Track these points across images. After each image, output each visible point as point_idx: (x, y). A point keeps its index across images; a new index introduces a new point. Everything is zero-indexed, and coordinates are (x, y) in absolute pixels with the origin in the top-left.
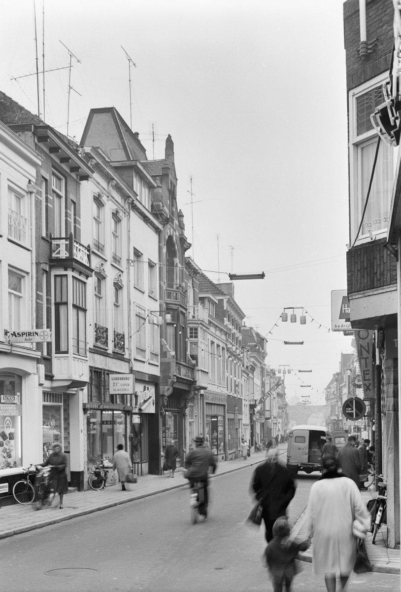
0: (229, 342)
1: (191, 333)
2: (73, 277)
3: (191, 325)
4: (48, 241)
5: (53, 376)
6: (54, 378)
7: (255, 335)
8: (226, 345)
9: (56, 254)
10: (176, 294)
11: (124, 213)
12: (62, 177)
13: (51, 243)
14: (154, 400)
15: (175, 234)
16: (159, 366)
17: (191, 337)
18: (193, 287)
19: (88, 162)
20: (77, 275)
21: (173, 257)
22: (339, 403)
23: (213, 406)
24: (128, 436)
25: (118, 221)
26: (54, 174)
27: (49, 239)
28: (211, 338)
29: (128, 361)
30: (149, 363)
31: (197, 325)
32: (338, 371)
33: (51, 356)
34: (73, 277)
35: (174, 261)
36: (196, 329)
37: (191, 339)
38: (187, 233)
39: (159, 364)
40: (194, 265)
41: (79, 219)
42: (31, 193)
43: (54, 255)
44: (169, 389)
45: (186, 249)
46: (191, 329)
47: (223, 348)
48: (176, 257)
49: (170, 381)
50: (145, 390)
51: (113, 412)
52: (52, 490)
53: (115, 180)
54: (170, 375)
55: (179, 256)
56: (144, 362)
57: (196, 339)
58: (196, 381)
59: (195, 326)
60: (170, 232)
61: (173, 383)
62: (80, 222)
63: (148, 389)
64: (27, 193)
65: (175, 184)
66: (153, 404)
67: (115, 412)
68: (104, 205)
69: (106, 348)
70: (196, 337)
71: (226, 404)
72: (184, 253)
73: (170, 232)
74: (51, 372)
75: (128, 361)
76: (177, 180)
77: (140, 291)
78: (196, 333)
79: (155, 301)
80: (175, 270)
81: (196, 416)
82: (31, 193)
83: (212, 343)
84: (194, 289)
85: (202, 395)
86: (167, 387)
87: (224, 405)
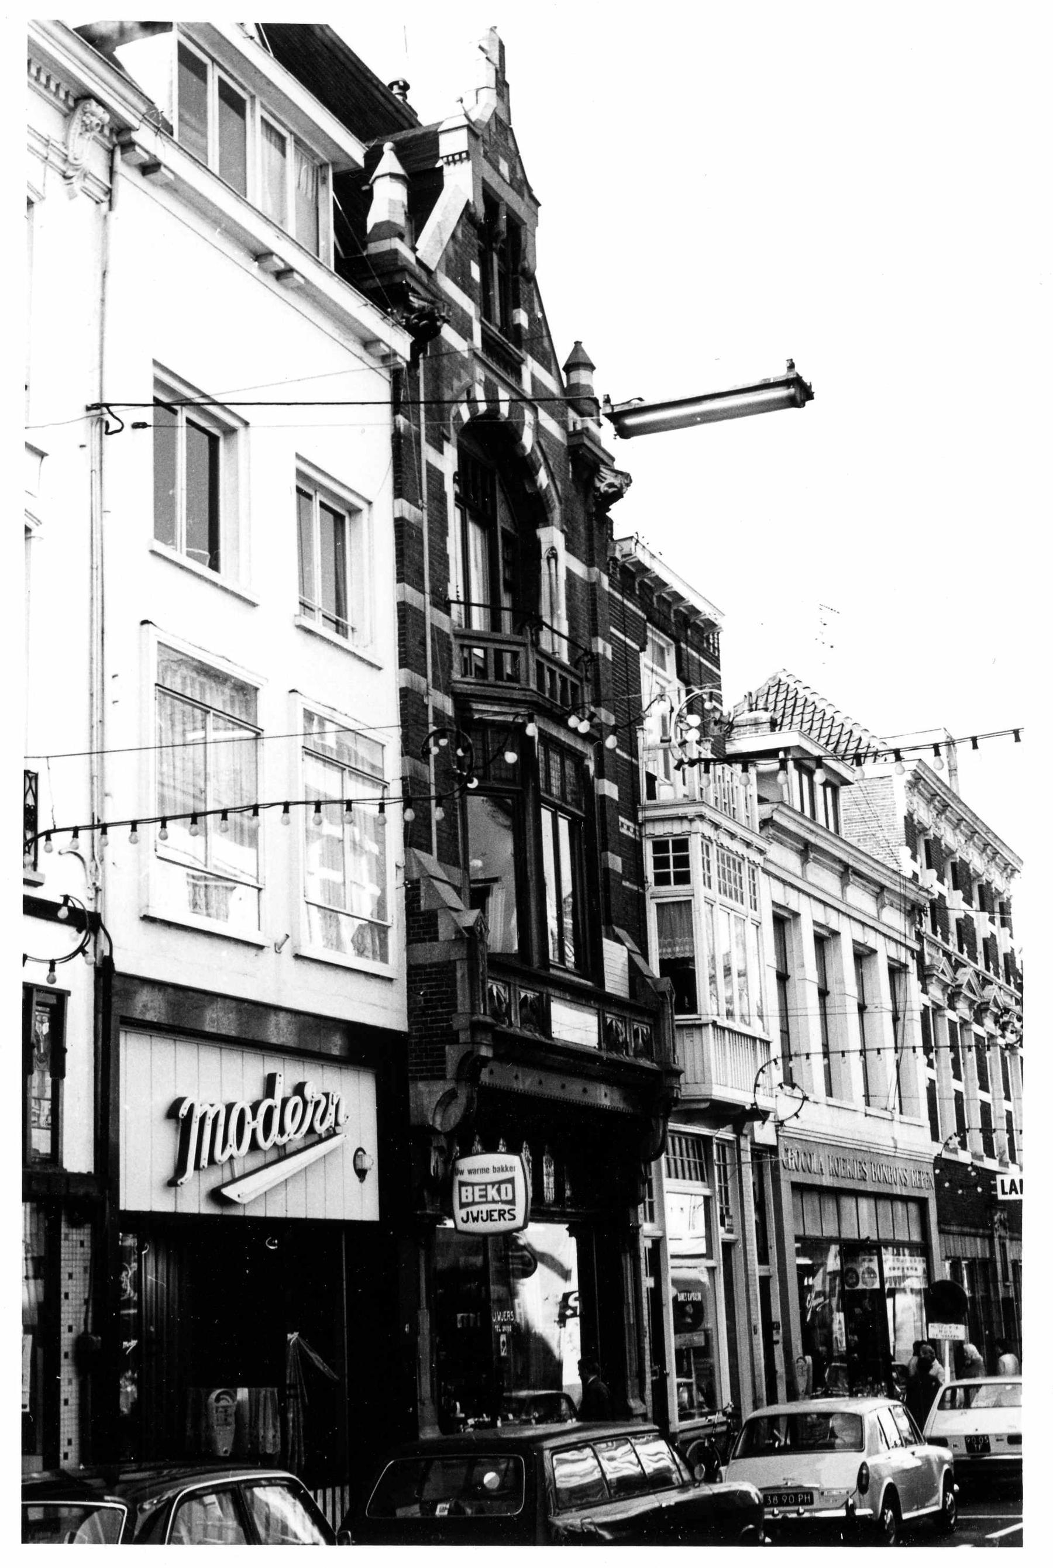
0: (933, 944)
1: (660, 863)
3: (659, 829)
8: (919, 957)
10: (515, 655)
15: (528, 416)
17: (662, 880)
23: (848, 1203)
24: (67, 1340)
28: (770, 892)
31: (686, 826)
35: (537, 543)
36: (682, 845)
37: (663, 889)
44: (450, 1097)
46: (660, 846)
47: (896, 971)
48: (547, 523)
49: (453, 1054)
52: (870, 1379)
53: (100, 103)
56: (261, 947)
57: (681, 888)
58: (678, 1073)
59: (677, 828)
61: (471, 1066)
65: (519, 206)
66: (361, 1173)
70: (683, 878)
71: (931, 1195)
73: (493, 400)
76: (538, 204)
77: (361, 659)
78: (683, 861)
79: (375, 670)
83: (783, 920)
85: (761, 1152)
86: (440, 1089)
87: (922, 1203)
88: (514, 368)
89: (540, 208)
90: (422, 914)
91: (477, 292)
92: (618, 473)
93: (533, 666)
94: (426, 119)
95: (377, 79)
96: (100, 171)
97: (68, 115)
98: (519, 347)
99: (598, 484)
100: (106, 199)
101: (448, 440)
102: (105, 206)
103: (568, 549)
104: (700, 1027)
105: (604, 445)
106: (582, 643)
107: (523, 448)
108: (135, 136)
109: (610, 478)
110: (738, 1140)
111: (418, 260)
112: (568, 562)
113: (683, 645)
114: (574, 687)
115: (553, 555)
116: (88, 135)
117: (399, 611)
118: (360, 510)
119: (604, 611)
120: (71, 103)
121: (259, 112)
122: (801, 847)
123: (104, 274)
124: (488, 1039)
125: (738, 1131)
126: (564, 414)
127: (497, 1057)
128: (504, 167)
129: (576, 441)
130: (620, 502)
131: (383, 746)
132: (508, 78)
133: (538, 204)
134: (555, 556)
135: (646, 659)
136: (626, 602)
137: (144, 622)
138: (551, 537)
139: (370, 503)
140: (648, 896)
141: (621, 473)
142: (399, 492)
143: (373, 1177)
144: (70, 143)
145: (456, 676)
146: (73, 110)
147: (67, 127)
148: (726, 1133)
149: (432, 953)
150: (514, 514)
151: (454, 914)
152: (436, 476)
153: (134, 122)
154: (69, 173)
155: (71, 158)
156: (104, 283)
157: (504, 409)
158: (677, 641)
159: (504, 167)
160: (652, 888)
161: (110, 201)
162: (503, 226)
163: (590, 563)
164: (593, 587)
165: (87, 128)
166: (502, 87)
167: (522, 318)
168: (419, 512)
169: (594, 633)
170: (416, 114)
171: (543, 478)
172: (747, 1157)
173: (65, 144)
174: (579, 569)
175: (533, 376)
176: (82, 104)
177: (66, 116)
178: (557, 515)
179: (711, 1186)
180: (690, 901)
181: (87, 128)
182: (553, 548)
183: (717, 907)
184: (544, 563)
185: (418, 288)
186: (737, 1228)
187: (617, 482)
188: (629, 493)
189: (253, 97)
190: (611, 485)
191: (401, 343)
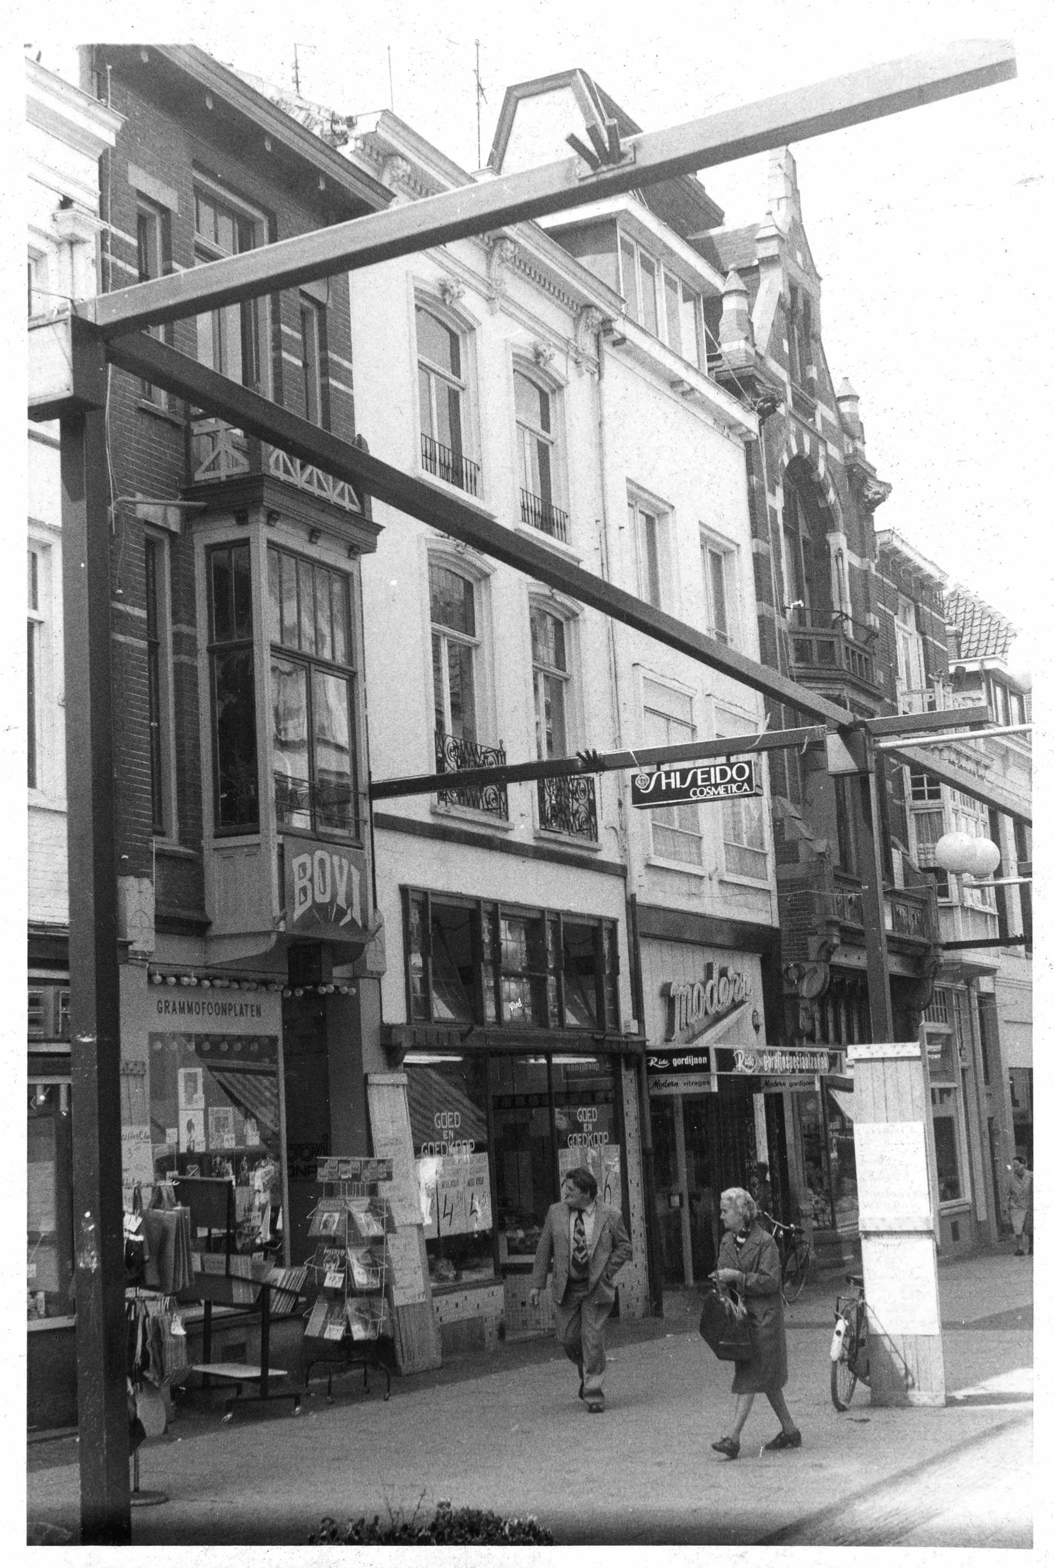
1: (917, 783)
2: (272, 545)
4: (175, 425)
5: (209, 924)
6: (214, 930)
7: (777, 630)
9: (204, 472)
11: (577, 363)
12: (257, 214)
13: (188, 434)
14: (761, 1009)
15: (822, 452)
16: (775, 893)
17: (918, 795)
18: (923, 633)
19: (380, 173)
20: (294, 539)
21: (825, 532)
22: (145, 918)
25: (553, 392)
26: (200, 192)
27: (180, 420)
29: (621, 872)
30: (721, 882)
32: (882, 518)
33: (200, 849)
34: (272, 545)
35: (827, 543)
37: (919, 803)
38: (872, 454)
39: (771, 884)
40: (911, 555)
41: (346, 364)
42: (73, 242)
43: (200, 476)
45: (874, 503)
48: (834, 528)
50: (709, 976)
51: (549, 1060)
54: (816, 921)
55: (847, 526)
56: (701, 878)
60: (800, 444)
62: (350, 372)
63: (723, 973)
64: (59, 244)
66: (757, 1027)
67: (557, 1060)
68: (472, 329)
69: (505, 825)
72: (871, 520)
73: (800, 444)
74: (201, 907)
75: (621, 872)
80: (834, 574)
81: (963, 1070)
82: (73, 242)
84: (925, 643)
88: (810, 413)
89: (822, 282)
90: (787, 843)
91: (787, 363)
92: (882, 484)
93: (843, 651)
94: (699, 172)
95: (713, 203)
96: (591, 351)
97: (576, 320)
98: (813, 396)
99: (867, 493)
100: (596, 370)
101: (778, 484)
102: (596, 376)
103: (849, 548)
104: (951, 908)
105: (868, 459)
106: (860, 619)
107: (819, 475)
108: (614, 325)
109: (876, 489)
110: (968, 989)
111: (756, 352)
112: (850, 558)
113: (920, 604)
114: (866, 660)
115: (840, 554)
116: (504, 266)
117: (759, 622)
118: (733, 551)
119: (873, 594)
120: (491, 243)
121: (662, 269)
122: (1003, 753)
123: (600, 424)
124: (836, 932)
125: (968, 983)
126: (841, 439)
127: (843, 942)
128: (799, 257)
129: (851, 461)
130: (883, 505)
131: (691, 698)
132: (799, 187)
133: (820, 279)
134: (841, 555)
135: (897, 621)
136: (885, 580)
137: (634, 665)
138: (838, 540)
139: (738, 545)
140: (907, 809)
141: (885, 484)
142: (755, 535)
143: (763, 1029)
144: (579, 338)
145: (792, 663)
146: (493, 248)
147: (576, 327)
148: (961, 986)
149: (799, 871)
150: (811, 528)
151: (810, 843)
152: (774, 512)
153: (614, 316)
154: (580, 360)
155: (580, 350)
156: (600, 433)
157: (807, 450)
158: (916, 602)
159: (799, 257)
160: (909, 802)
161: (599, 371)
162: (800, 305)
163: (862, 556)
164: (866, 573)
165: (503, 260)
166: (795, 195)
167: (813, 373)
168: (766, 545)
169: (868, 610)
170: (703, 187)
171: (832, 496)
172: (975, 1003)
173: (575, 340)
174: (856, 561)
175: (823, 417)
176: (499, 243)
177: (574, 319)
178: (841, 523)
179: (952, 1026)
180: (941, 813)
181: (503, 260)
182: (840, 549)
183: (960, 814)
184: (833, 561)
185: (762, 378)
186: (970, 1058)
187: (881, 490)
188: (891, 497)
189: (658, 260)
190: (877, 493)
191: (751, 422)
